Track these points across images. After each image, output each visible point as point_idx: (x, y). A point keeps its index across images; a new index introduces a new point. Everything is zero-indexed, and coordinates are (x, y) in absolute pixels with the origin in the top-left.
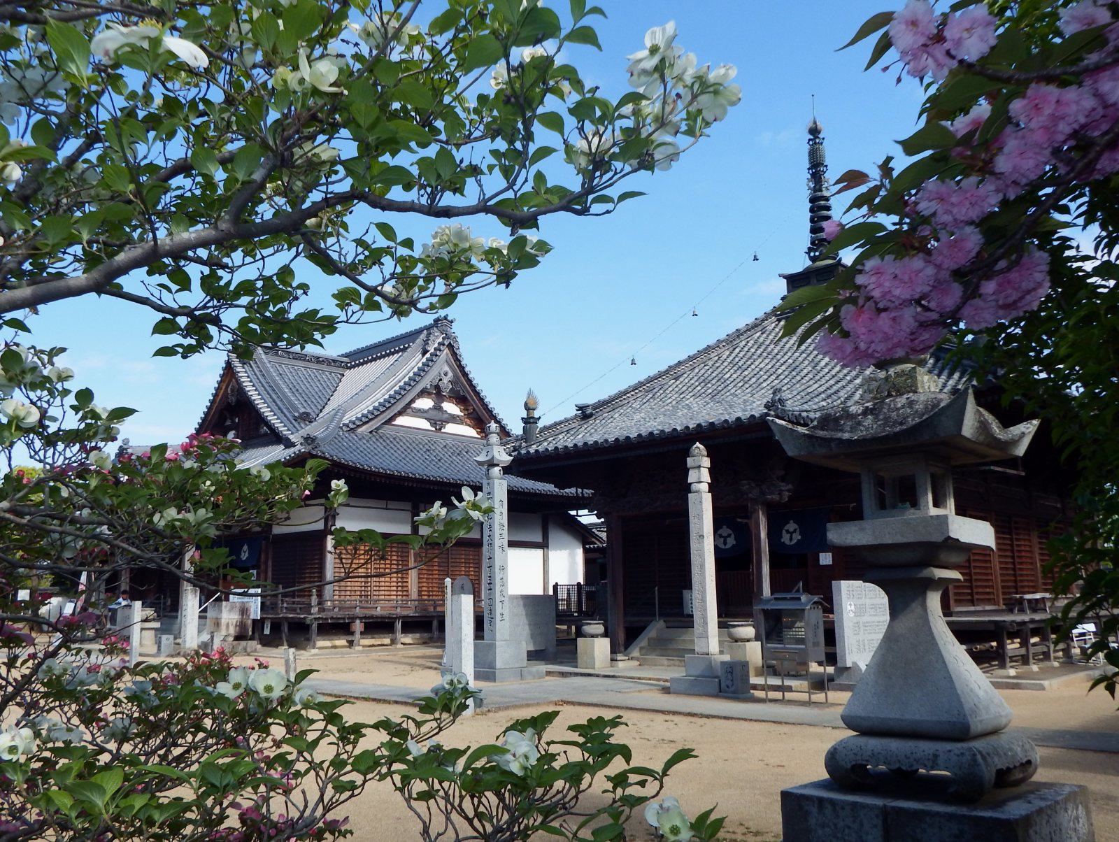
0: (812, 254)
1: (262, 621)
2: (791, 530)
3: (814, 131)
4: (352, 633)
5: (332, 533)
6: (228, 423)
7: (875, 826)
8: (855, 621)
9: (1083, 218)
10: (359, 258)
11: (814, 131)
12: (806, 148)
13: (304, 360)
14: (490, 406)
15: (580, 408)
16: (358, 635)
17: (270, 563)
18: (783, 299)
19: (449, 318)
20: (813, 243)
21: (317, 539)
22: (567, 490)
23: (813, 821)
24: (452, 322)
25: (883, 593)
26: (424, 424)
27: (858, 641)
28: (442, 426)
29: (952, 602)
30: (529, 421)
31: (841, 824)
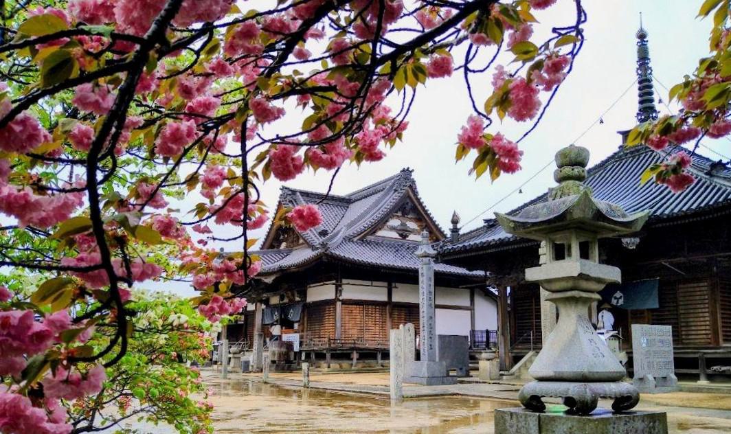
0: (639, 118)
1: (300, 352)
2: (618, 297)
3: (642, 36)
4: (352, 359)
5: (339, 300)
6: (282, 237)
7: (535, 425)
8: (647, 350)
9: (226, 28)
10: (15, 68)
11: (642, 36)
12: (636, 48)
13: (333, 200)
14: (437, 223)
15: (486, 221)
16: (355, 361)
17: (306, 319)
18: (620, 147)
19: (410, 170)
20: (640, 110)
21: (331, 303)
22: (475, 273)
23: (508, 424)
24: (411, 172)
25: (612, 316)
26: (395, 235)
27: (649, 362)
28: (407, 236)
29: (721, 340)
30: (455, 231)
31: (520, 425)
